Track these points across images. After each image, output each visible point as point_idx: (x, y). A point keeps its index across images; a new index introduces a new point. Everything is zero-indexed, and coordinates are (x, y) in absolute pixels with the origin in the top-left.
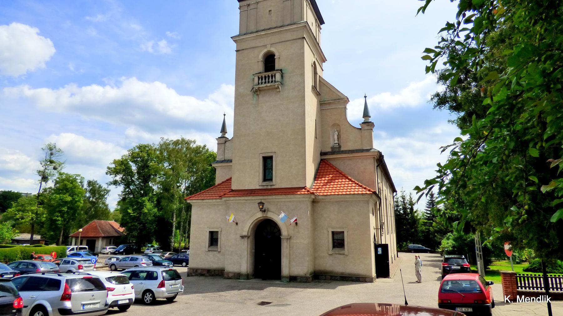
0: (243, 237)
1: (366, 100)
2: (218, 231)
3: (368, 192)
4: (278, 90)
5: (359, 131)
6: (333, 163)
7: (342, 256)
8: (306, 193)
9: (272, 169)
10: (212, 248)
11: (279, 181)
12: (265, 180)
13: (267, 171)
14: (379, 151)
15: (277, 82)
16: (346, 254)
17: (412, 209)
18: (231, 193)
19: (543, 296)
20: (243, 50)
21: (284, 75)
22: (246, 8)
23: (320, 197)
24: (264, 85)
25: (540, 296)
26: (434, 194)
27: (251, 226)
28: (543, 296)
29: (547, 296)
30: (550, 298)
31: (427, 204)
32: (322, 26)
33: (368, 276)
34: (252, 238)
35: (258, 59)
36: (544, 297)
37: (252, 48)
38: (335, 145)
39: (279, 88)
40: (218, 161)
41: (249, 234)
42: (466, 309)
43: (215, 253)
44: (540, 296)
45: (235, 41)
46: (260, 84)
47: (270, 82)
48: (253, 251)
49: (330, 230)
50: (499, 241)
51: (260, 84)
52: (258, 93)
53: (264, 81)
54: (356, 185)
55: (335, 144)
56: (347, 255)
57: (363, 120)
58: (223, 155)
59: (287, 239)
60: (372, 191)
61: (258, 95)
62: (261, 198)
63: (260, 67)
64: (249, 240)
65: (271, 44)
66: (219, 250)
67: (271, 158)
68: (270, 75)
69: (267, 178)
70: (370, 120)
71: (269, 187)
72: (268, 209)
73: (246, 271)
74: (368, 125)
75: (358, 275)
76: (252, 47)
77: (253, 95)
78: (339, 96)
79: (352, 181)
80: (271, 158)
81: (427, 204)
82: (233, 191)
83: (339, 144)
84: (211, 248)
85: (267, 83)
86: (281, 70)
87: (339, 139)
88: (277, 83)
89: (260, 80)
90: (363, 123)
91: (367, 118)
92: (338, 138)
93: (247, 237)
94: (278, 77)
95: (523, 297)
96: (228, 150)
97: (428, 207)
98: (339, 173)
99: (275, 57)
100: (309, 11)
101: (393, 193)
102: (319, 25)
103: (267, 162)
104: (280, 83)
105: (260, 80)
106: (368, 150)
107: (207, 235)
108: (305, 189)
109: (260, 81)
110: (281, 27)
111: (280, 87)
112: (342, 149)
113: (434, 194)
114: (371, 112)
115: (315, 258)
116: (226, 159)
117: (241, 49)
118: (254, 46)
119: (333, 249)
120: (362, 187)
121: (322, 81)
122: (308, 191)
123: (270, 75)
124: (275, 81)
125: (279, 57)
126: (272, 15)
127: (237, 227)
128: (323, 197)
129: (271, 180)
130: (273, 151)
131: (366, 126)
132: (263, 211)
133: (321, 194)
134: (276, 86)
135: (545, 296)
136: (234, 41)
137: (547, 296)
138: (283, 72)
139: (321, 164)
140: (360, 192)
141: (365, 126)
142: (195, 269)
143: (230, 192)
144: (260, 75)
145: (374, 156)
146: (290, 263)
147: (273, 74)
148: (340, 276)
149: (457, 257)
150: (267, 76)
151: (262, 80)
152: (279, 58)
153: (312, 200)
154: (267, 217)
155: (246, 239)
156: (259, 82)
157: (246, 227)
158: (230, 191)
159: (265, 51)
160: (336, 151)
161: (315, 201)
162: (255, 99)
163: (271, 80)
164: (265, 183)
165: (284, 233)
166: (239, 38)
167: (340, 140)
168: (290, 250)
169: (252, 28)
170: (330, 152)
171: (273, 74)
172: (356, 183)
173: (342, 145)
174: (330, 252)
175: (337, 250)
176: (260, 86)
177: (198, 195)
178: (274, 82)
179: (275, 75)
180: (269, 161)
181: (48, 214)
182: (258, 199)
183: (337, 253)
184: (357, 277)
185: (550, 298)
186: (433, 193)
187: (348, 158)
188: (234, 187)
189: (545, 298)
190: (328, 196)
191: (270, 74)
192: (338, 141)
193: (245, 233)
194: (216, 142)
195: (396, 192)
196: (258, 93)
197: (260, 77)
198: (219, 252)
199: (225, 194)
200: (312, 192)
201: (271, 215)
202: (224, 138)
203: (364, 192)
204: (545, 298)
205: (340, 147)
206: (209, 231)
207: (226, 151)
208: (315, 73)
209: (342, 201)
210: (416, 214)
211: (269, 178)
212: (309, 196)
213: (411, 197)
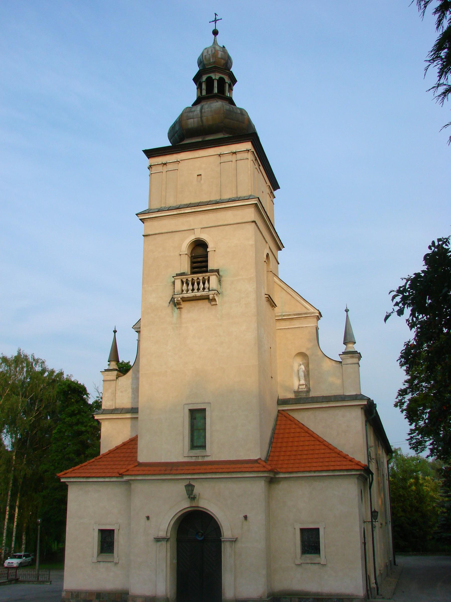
0: (158, 540)
1: (347, 316)
2: (113, 530)
4: (213, 303)
5: (338, 365)
7: (316, 567)
9: (205, 429)
10: (105, 556)
12: (193, 446)
14: (370, 399)
15: (212, 290)
18: (137, 468)
21: (222, 279)
32: (275, 193)
33: (357, 596)
34: (173, 540)
37: (170, 232)
38: (300, 387)
41: (169, 535)
42: (14, 531)
43: (109, 564)
46: (185, 292)
47: (201, 289)
48: (175, 561)
49: (298, 527)
51: (185, 292)
53: (190, 287)
54: (332, 451)
55: (300, 385)
57: (343, 348)
58: (112, 400)
59: (232, 541)
64: (169, 545)
65: (201, 228)
66: (116, 560)
69: (195, 445)
70: (356, 347)
71: (200, 460)
72: (199, 494)
73: (164, 593)
74: (352, 357)
75: (341, 595)
76: (170, 231)
77: (173, 309)
80: (203, 411)
82: (140, 464)
85: (196, 291)
86: (217, 271)
88: (213, 292)
89: (185, 285)
91: (350, 345)
93: (166, 539)
94: (213, 279)
96: (122, 392)
98: (308, 435)
99: (208, 250)
102: (271, 192)
105: (185, 285)
110: (217, 203)
112: (312, 394)
116: (118, 406)
118: (174, 230)
119: (301, 556)
124: (209, 288)
126: (202, 182)
127: (148, 523)
129: (203, 447)
130: (206, 401)
132: (192, 498)
136: (140, 219)
139: (279, 418)
142: (75, 592)
143: (136, 466)
144: (184, 278)
147: (206, 278)
148: (314, 598)
149: (345, 356)
151: (188, 284)
154: (198, 507)
155: (164, 543)
158: (136, 464)
159: (192, 238)
163: (203, 286)
164: (197, 452)
166: (149, 217)
174: (298, 562)
175: (309, 557)
177: (79, 469)
178: (206, 290)
179: (209, 277)
180: (198, 415)
181: (5, 544)
183: (309, 561)
184: (339, 599)
191: (200, 276)
193: (162, 534)
194: (101, 377)
197: (184, 280)
198: (116, 564)
199: (128, 470)
205: (308, 391)
206: (99, 530)
211: (199, 444)
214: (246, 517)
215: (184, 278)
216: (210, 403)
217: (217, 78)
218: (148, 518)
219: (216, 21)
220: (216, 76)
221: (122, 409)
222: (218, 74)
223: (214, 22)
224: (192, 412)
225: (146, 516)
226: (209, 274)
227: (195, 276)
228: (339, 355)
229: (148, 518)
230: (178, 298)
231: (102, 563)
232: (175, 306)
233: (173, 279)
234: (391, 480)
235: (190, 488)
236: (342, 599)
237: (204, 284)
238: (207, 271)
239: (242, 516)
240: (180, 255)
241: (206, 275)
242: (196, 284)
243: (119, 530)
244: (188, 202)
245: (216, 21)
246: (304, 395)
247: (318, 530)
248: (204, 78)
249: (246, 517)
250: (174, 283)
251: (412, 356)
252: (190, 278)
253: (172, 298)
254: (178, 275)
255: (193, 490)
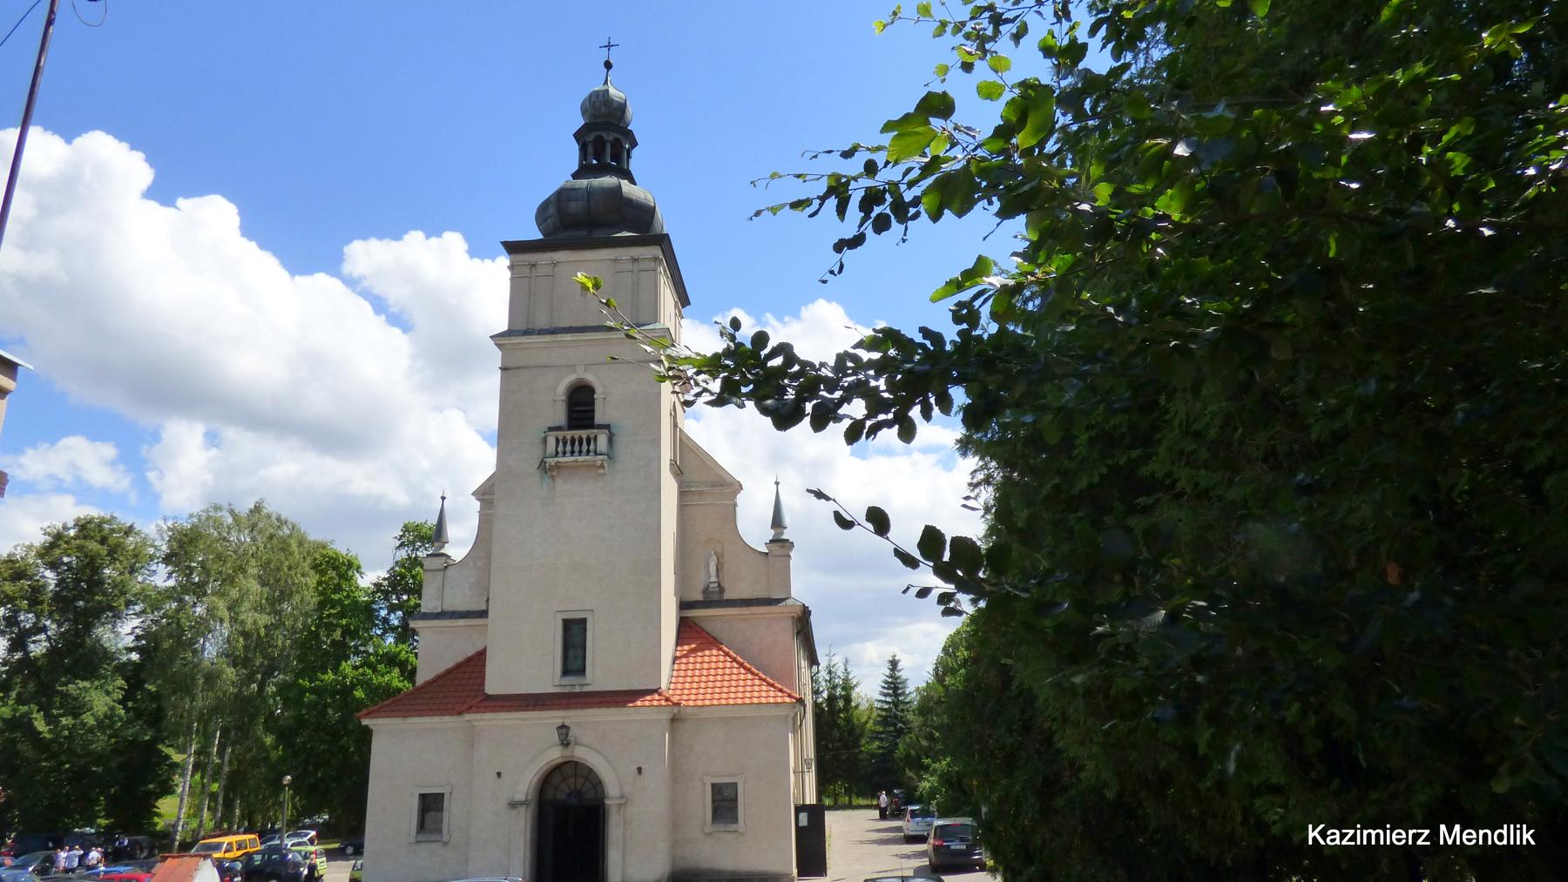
0: (513, 805)
2: (443, 794)
3: (788, 700)
4: (601, 471)
6: (708, 627)
8: (663, 703)
11: (598, 678)
12: (566, 672)
13: (571, 653)
15: (602, 454)
16: (740, 831)
17: (848, 699)
19: (1512, 826)
20: (519, 368)
22: (526, 271)
23: (689, 710)
24: (569, 459)
25: (1505, 826)
26: (899, 660)
27: (534, 782)
28: (1512, 826)
29: (1525, 826)
30: (1532, 831)
31: (883, 687)
35: (556, 395)
36: (1515, 829)
39: (604, 467)
40: (424, 614)
43: (434, 846)
44: (1505, 826)
45: (500, 346)
46: (561, 454)
49: (709, 781)
50: (1346, 211)
51: (561, 454)
52: (555, 474)
53: (569, 448)
56: (742, 834)
60: (795, 698)
61: (552, 477)
62: (561, 713)
63: (559, 415)
66: (445, 838)
67: (582, 623)
68: (584, 437)
71: (577, 690)
74: (783, 547)
77: (542, 477)
78: (720, 476)
79: (752, 673)
80: (583, 622)
81: (883, 687)
82: (489, 697)
83: (719, 585)
84: (421, 838)
85: (576, 454)
86: (607, 427)
87: (720, 572)
88: (601, 457)
89: (561, 444)
90: (771, 541)
91: (779, 530)
92: (717, 571)
94: (602, 440)
95: (1457, 828)
97: (886, 695)
99: (595, 396)
100: (668, 292)
101: (811, 667)
103: (574, 633)
104: (606, 457)
105: (561, 444)
106: (778, 601)
107: (415, 803)
108: (660, 694)
109: (560, 449)
111: (606, 465)
112: (727, 596)
113: (899, 660)
114: (787, 519)
115: (675, 844)
117: (515, 365)
120: (774, 687)
121: (686, 441)
122: (667, 700)
123: (584, 437)
125: (604, 396)
128: (695, 710)
129: (582, 671)
130: (588, 608)
131: (778, 548)
133: (691, 703)
134: (599, 463)
135: (1518, 826)
137: (1525, 826)
138: (613, 430)
140: (771, 700)
141: (775, 547)
143: (482, 701)
145: (792, 615)
146: (624, 857)
147: (592, 436)
150: (577, 437)
152: (604, 399)
153: (670, 717)
156: (559, 449)
157: (524, 783)
158: (484, 697)
160: (714, 599)
161: (676, 717)
162: (544, 485)
164: (570, 680)
165: (612, 789)
167: (721, 575)
168: (625, 829)
169: (542, 322)
170: (700, 602)
171: (592, 436)
172: (760, 679)
173: (726, 586)
174: (707, 831)
176: (562, 459)
180: (575, 629)
182: (555, 717)
185: (1532, 831)
186: (897, 658)
187: (738, 617)
188: (492, 687)
189: (1518, 832)
190: (706, 709)
191: (584, 434)
192: (718, 576)
193: (520, 797)
195: (818, 664)
196: (555, 474)
197: (561, 438)
198: (446, 843)
200: (676, 701)
201: (581, 754)
202: (444, 558)
203: (779, 700)
204: (1518, 832)
205: (722, 590)
206: (420, 795)
207: (447, 590)
208: (675, 425)
209: (734, 718)
210: (856, 713)
212: (669, 709)
213: (846, 670)
214: (640, 770)
215: (561, 434)
216: (593, 611)
217: (611, 138)
218: (499, 774)
219: (609, 46)
220: (609, 136)
221: (454, 612)
222: (611, 133)
223: (607, 48)
224: (567, 624)
225: (907, 680)
226: (595, 431)
227: (577, 433)
228: (766, 544)
229: (499, 774)
230: (551, 461)
231: (423, 845)
232: (546, 472)
233: (543, 435)
234: (291, 792)
235: (564, 731)
236: (766, 879)
237: (589, 444)
238: (592, 426)
239: (634, 768)
240: (555, 401)
241: (592, 433)
242: (577, 443)
243: (451, 793)
244: (567, 325)
245: (609, 46)
246: (716, 597)
247: (736, 784)
248: (591, 137)
249: (640, 770)
250: (545, 440)
251: (1124, 318)
252: (569, 434)
253: (542, 461)
254: (551, 429)
255: (567, 734)
